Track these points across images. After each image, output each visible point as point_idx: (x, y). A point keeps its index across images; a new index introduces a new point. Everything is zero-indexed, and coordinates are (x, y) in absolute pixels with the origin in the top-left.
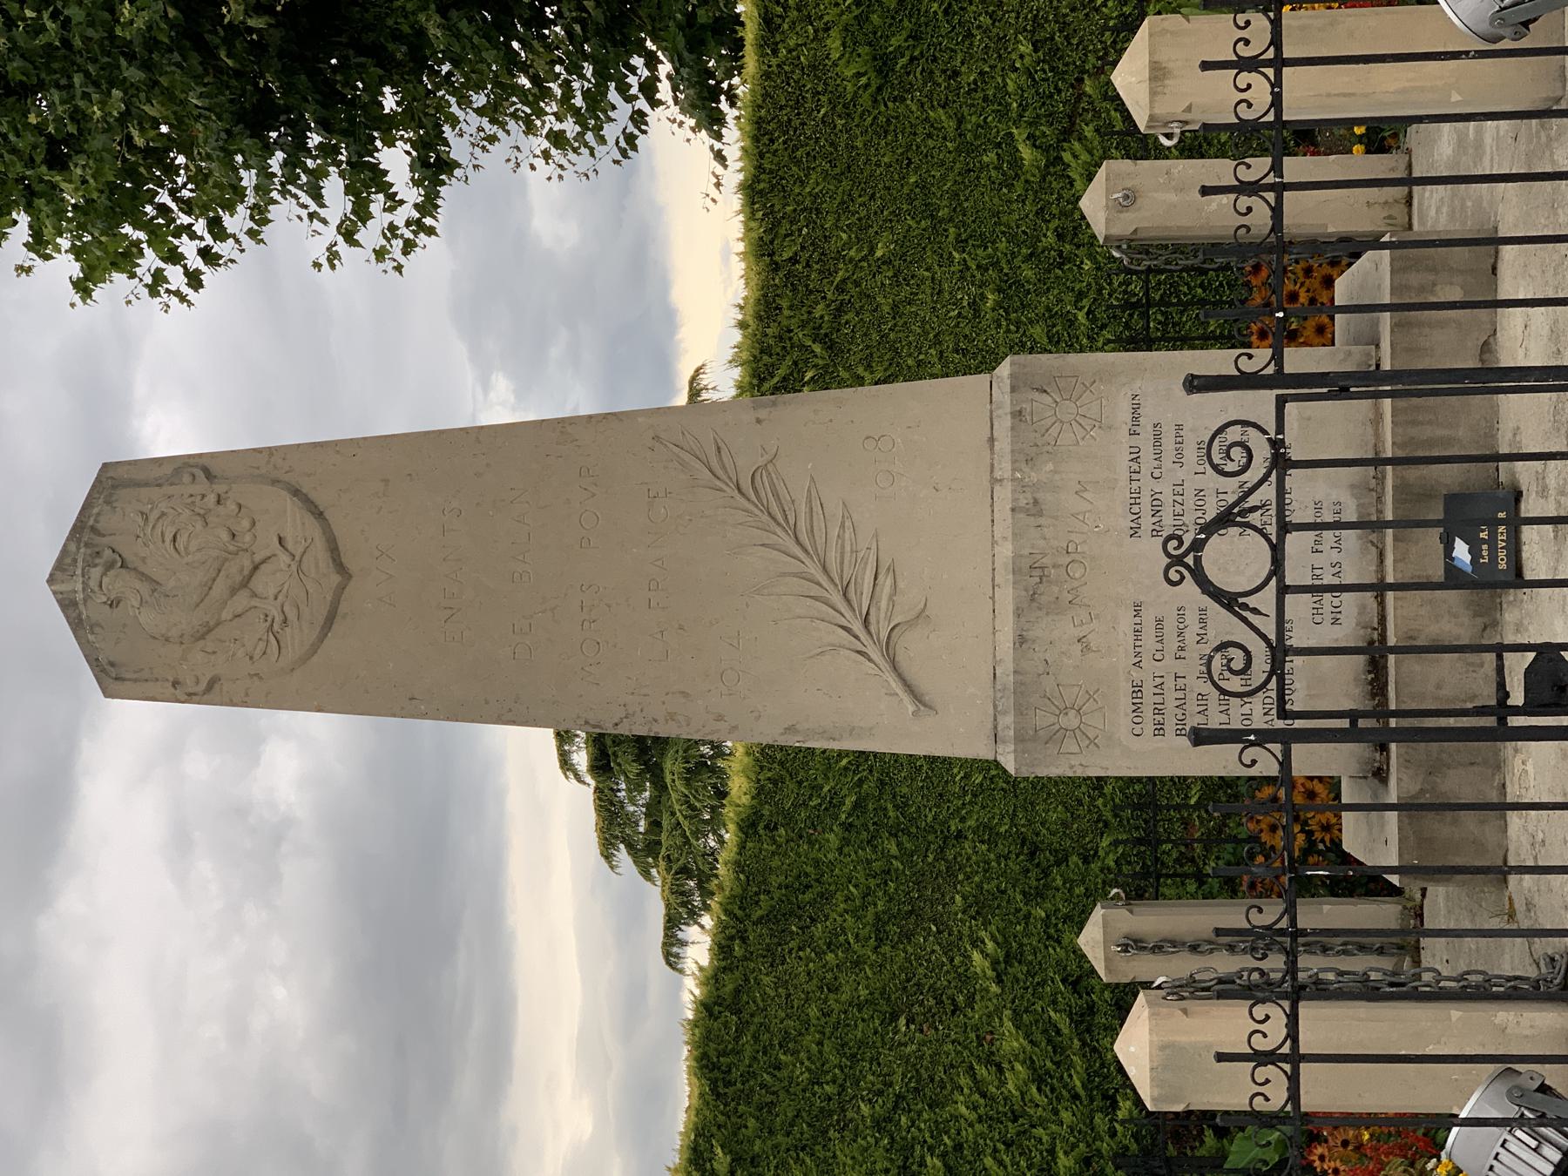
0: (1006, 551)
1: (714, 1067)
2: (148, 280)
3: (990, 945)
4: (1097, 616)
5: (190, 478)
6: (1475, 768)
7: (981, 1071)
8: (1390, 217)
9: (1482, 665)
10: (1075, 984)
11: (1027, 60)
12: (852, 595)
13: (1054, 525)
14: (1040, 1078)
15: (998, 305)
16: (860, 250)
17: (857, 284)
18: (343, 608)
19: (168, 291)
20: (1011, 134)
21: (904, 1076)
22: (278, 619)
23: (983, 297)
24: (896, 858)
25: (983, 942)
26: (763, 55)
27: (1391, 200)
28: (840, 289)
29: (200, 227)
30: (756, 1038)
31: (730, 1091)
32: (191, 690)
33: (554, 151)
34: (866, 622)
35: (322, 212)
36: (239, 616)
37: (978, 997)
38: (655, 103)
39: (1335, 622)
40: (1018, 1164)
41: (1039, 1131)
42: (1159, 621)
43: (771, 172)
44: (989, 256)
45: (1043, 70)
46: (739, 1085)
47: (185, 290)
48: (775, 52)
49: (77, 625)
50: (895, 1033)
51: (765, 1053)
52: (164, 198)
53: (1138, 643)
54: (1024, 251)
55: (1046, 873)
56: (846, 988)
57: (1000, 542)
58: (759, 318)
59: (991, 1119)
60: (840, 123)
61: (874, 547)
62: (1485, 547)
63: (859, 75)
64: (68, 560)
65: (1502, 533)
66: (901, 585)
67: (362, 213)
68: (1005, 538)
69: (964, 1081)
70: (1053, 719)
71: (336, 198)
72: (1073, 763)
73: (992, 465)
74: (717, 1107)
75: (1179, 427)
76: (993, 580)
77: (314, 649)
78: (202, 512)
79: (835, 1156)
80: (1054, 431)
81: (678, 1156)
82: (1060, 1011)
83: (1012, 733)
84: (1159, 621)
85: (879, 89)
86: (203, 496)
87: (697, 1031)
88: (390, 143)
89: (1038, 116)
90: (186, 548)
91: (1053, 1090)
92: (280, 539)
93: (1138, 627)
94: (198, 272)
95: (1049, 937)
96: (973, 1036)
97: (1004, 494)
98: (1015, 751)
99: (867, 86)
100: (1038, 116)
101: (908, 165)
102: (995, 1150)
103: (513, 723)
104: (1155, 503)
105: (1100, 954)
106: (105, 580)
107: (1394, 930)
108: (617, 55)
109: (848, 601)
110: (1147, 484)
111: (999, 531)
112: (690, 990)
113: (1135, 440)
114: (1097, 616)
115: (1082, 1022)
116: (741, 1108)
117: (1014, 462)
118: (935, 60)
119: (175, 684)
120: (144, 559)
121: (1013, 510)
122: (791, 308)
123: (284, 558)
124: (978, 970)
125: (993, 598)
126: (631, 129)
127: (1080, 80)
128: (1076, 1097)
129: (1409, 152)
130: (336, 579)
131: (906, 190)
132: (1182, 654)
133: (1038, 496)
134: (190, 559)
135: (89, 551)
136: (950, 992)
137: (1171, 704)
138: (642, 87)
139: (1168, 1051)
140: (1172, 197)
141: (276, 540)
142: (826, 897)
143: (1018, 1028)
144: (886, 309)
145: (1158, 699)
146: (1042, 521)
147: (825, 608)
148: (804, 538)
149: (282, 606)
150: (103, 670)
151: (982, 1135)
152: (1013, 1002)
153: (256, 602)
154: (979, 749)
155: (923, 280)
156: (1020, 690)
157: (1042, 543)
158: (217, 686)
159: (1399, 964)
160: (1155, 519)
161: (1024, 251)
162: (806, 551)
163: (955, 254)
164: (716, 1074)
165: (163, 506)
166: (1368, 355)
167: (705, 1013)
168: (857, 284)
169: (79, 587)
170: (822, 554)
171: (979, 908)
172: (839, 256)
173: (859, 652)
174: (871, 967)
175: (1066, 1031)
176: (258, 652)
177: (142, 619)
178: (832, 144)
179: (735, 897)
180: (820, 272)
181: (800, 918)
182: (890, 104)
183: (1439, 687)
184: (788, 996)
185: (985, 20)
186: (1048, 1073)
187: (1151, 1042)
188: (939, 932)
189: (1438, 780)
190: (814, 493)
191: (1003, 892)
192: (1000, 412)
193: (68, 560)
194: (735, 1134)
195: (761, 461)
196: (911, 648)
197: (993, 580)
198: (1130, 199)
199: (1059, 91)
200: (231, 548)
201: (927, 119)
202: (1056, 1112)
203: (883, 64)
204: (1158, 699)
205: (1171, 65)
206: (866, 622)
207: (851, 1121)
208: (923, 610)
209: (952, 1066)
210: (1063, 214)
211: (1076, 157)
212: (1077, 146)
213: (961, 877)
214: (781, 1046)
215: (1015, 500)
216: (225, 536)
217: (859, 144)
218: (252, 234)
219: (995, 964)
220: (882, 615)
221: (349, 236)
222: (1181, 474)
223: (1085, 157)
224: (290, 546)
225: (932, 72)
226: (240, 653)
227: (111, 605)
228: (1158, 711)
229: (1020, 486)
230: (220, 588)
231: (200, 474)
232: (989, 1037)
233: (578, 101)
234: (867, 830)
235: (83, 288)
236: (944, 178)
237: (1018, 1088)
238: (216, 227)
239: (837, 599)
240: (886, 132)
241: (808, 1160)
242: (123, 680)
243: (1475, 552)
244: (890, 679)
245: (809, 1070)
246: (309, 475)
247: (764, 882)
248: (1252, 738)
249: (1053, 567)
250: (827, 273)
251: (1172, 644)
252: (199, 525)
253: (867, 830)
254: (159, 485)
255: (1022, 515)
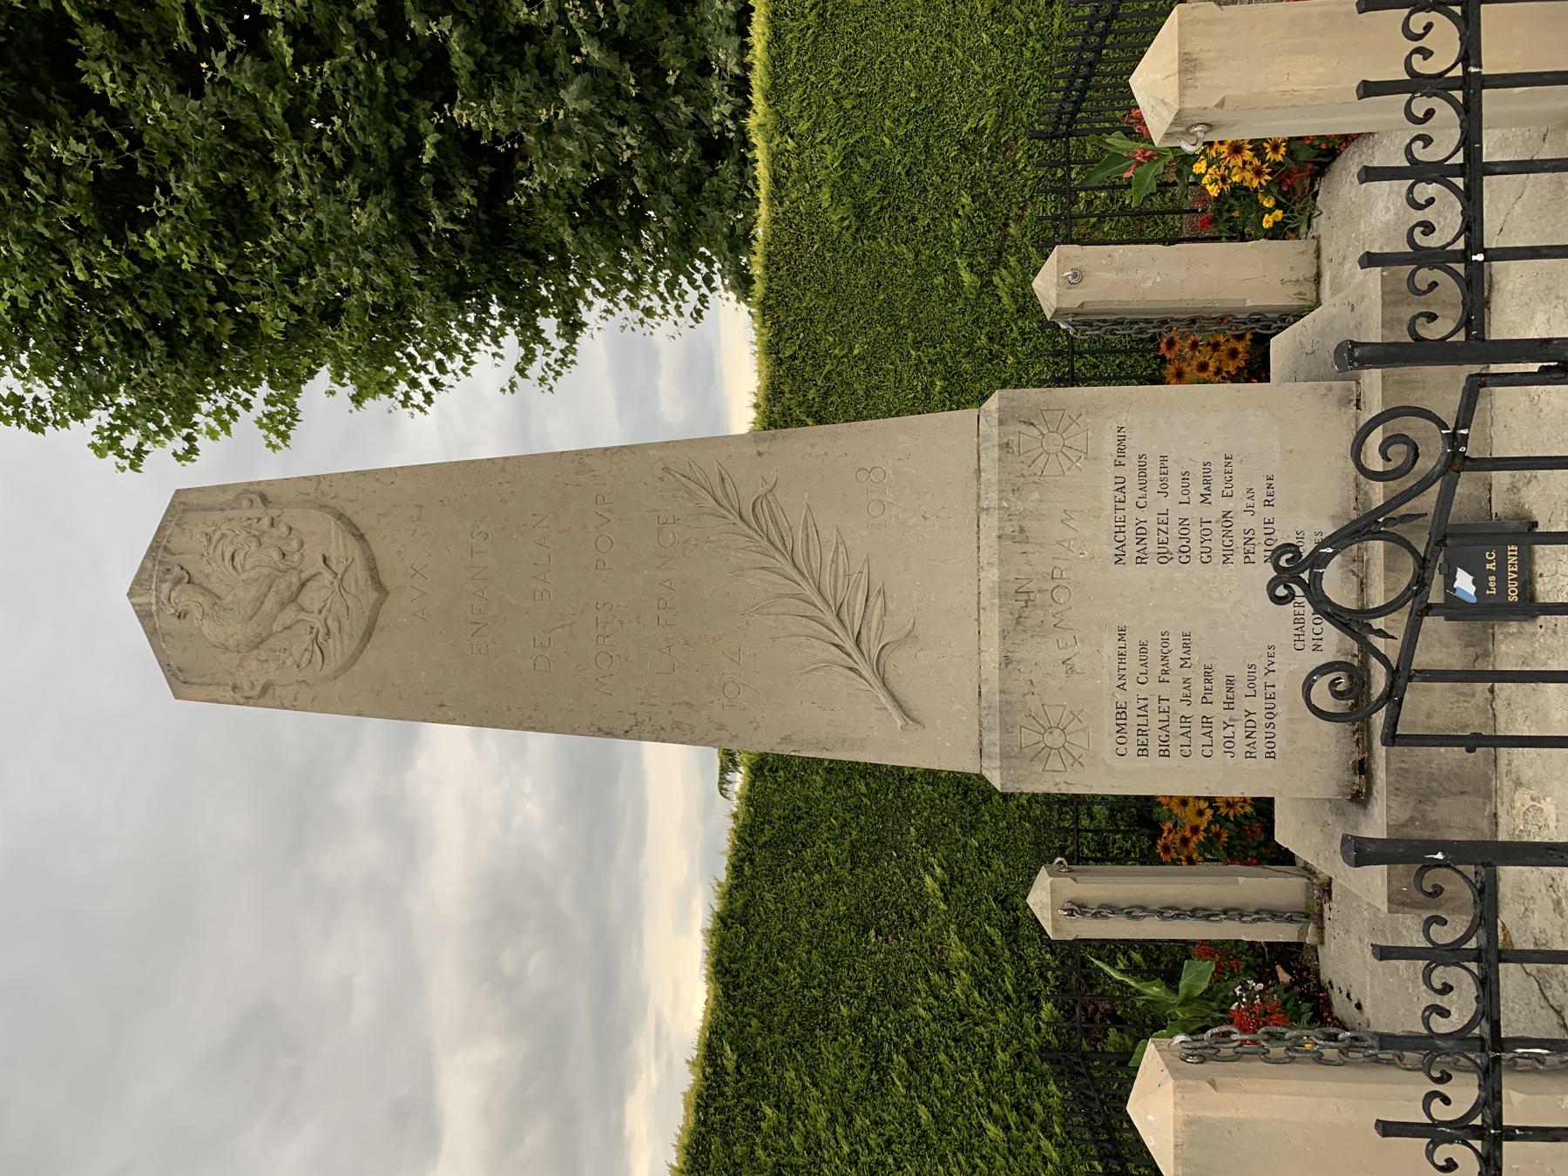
0: (992, 575)
1: (728, 971)
2: (402, 398)
3: (938, 870)
4: (1082, 640)
5: (248, 503)
6: (1466, 797)
7: (934, 977)
8: (1299, 293)
9: (1473, 695)
10: (1002, 902)
11: (967, 208)
12: (845, 617)
13: (1040, 552)
14: (980, 984)
15: (944, 389)
16: (842, 349)
17: (840, 374)
18: (381, 621)
19: (413, 405)
20: (955, 263)
21: (874, 981)
22: (322, 631)
23: (933, 384)
24: (864, 795)
25: (932, 866)
26: (773, 206)
27: (1302, 279)
28: (827, 378)
29: (431, 366)
30: (760, 947)
31: (738, 994)
32: (247, 694)
33: (646, 319)
34: (858, 641)
35: (501, 351)
36: (289, 627)
37: (930, 914)
38: (712, 290)
39: (1316, 648)
40: (965, 1058)
41: (980, 1029)
42: (1143, 646)
43: (778, 292)
44: (937, 354)
45: (979, 216)
46: (745, 988)
47: (423, 405)
48: (781, 203)
49: (152, 634)
50: (867, 943)
51: (766, 961)
52: (411, 350)
53: (1122, 666)
54: (963, 350)
55: (976, 809)
56: (829, 904)
57: (986, 567)
58: (769, 400)
59: (943, 1018)
60: (828, 255)
61: (865, 571)
62: (1492, 578)
63: (843, 219)
64: (145, 576)
65: (1513, 565)
66: (891, 607)
67: (529, 357)
68: (991, 564)
69: (921, 986)
70: (1038, 737)
71: (511, 341)
72: (1057, 780)
73: (979, 496)
74: (727, 1008)
75: (1164, 458)
76: (979, 603)
77: (354, 658)
78: (257, 533)
79: (820, 1053)
80: (1040, 463)
81: (675, 1155)
82: (993, 926)
83: (997, 749)
84: (1143, 646)
85: (858, 230)
86: (259, 520)
87: (714, 939)
88: (546, 316)
89: (975, 250)
90: (243, 567)
91: (990, 993)
92: (325, 559)
93: (1122, 650)
94: (430, 393)
95: (982, 863)
96: (927, 946)
97: (990, 523)
98: (1001, 767)
99: (848, 228)
100: (975, 250)
101: (878, 286)
102: (947, 1046)
103: (533, 729)
104: (1139, 531)
105: (1050, 924)
106: (173, 594)
107: (1499, 1032)
108: (686, 257)
109: (841, 621)
110: (1132, 513)
111: (985, 556)
112: (734, 805)
113: (1120, 471)
114: (1082, 640)
115: (1010, 934)
116: (746, 1009)
117: (1001, 491)
118: (899, 209)
119: (235, 688)
120: (207, 576)
121: (999, 537)
122: (791, 392)
123: (328, 576)
124: (930, 890)
125: (978, 620)
126: (699, 306)
127: (1006, 225)
128: (1008, 998)
129: (1317, 238)
130: (373, 595)
131: (876, 305)
132: (1166, 677)
133: (1024, 524)
134: (245, 576)
135: (162, 568)
136: (908, 908)
137: (1154, 725)
138: (704, 279)
139: (1194, 1128)
140: (1113, 276)
141: (321, 560)
142: (813, 826)
143: (961, 940)
144: (861, 393)
145: (1142, 721)
146: (1027, 548)
147: (819, 627)
148: (800, 561)
149: (326, 619)
150: (174, 675)
151: (936, 1033)
152: (957, 917)
153: (302, 616)
154: (965, 763)
155: (888, 371)
156: (1006, 709)
157: (1027, 568)
158: (270, 691)
159: (1302, 933)
160: (1140, 547)
161: (963, 350)
162: (802, 574)
163: (913, 352)
164: (728, 978)
165: (224, 529)
166: (1349, 390)
167: (721, 924)
168: (840, 374)
169: (153, 600)
170: (816, 576)
171: (929, 839)
172: (827, 354)
173: (851, 669)
174: (848, 886)
175: (999, 943)
176: (304, 663)
177: (205, 630)
178: (822, 271)
179: (745, 826)
180: (813, 365)
181: (794, 843)
182: (865, 242)
183: (1429, 716)
184: (785, 909)
185: (936, 179)
186: (986, 978)
187: (1175, 1117)
188: (899, 857)
189: (1429, 808)
190: (810, 520)
191: (946, 825)
192: (986, 444)
193: (145, 576)
194: (741, 1032)
195: (762, 491)
196: (901, 666)
197: (979, 603)
198: (1078, 276)
199: (991, 232)
200: (282, 566)
201: (893, 253)
202: (993, 1013)
203: (861, 212)
204: (1142, 721)
205: (1203, 56)
206: (858, 641)
207: (833, 1020)
208: (911, 631)
209: (912, 972)
210: (993, 322)
211: (1003, 280)
212: (1004, 272)
213: (913, 812)
214: (779, 953)
215: (1001, 528)
216: (276, 555)
217: (842, 271)
218: (464, 370)
219: (942, 885)
220: (873, 635)
221: (521, 371)
222: (1165, 504)
223: (1009, 280)
224: (333, 565)
225: (896, 218)
226: (289, 662)
227: (179, 617)
228: (1142, 732)
229: (1007, 514)
230: (270, 602)
231: (257, 500)
232: (939, 947)
233: (662, 288)
234: (843, 772)
235: (357, 400)
236: (904, 295)
237: (963, 993)
238: (440, 365)
239: (830, 619)
240: (862, 262)
241: (799, 1058)
242: (192, 684)
243: (1480, 582)
244: (880, 695)
245: (800, 975)
246: (352, 501)
247: (768, 813)
248: (1439, 856)
249: (1039, 591)
250: (817, 367)
251: (1156, 668)
252: (254, 546)
253: (843, 772)
254: (222, 510)
255: (1008, 543)
